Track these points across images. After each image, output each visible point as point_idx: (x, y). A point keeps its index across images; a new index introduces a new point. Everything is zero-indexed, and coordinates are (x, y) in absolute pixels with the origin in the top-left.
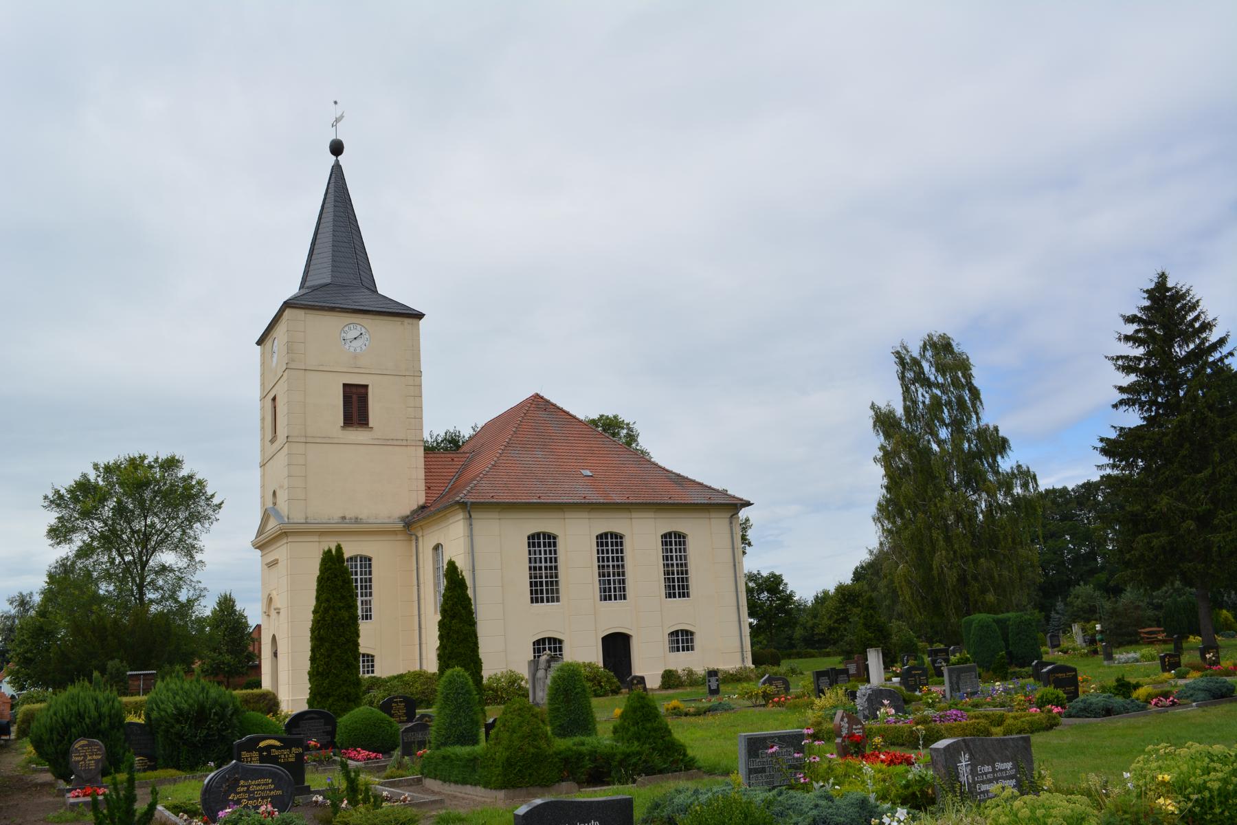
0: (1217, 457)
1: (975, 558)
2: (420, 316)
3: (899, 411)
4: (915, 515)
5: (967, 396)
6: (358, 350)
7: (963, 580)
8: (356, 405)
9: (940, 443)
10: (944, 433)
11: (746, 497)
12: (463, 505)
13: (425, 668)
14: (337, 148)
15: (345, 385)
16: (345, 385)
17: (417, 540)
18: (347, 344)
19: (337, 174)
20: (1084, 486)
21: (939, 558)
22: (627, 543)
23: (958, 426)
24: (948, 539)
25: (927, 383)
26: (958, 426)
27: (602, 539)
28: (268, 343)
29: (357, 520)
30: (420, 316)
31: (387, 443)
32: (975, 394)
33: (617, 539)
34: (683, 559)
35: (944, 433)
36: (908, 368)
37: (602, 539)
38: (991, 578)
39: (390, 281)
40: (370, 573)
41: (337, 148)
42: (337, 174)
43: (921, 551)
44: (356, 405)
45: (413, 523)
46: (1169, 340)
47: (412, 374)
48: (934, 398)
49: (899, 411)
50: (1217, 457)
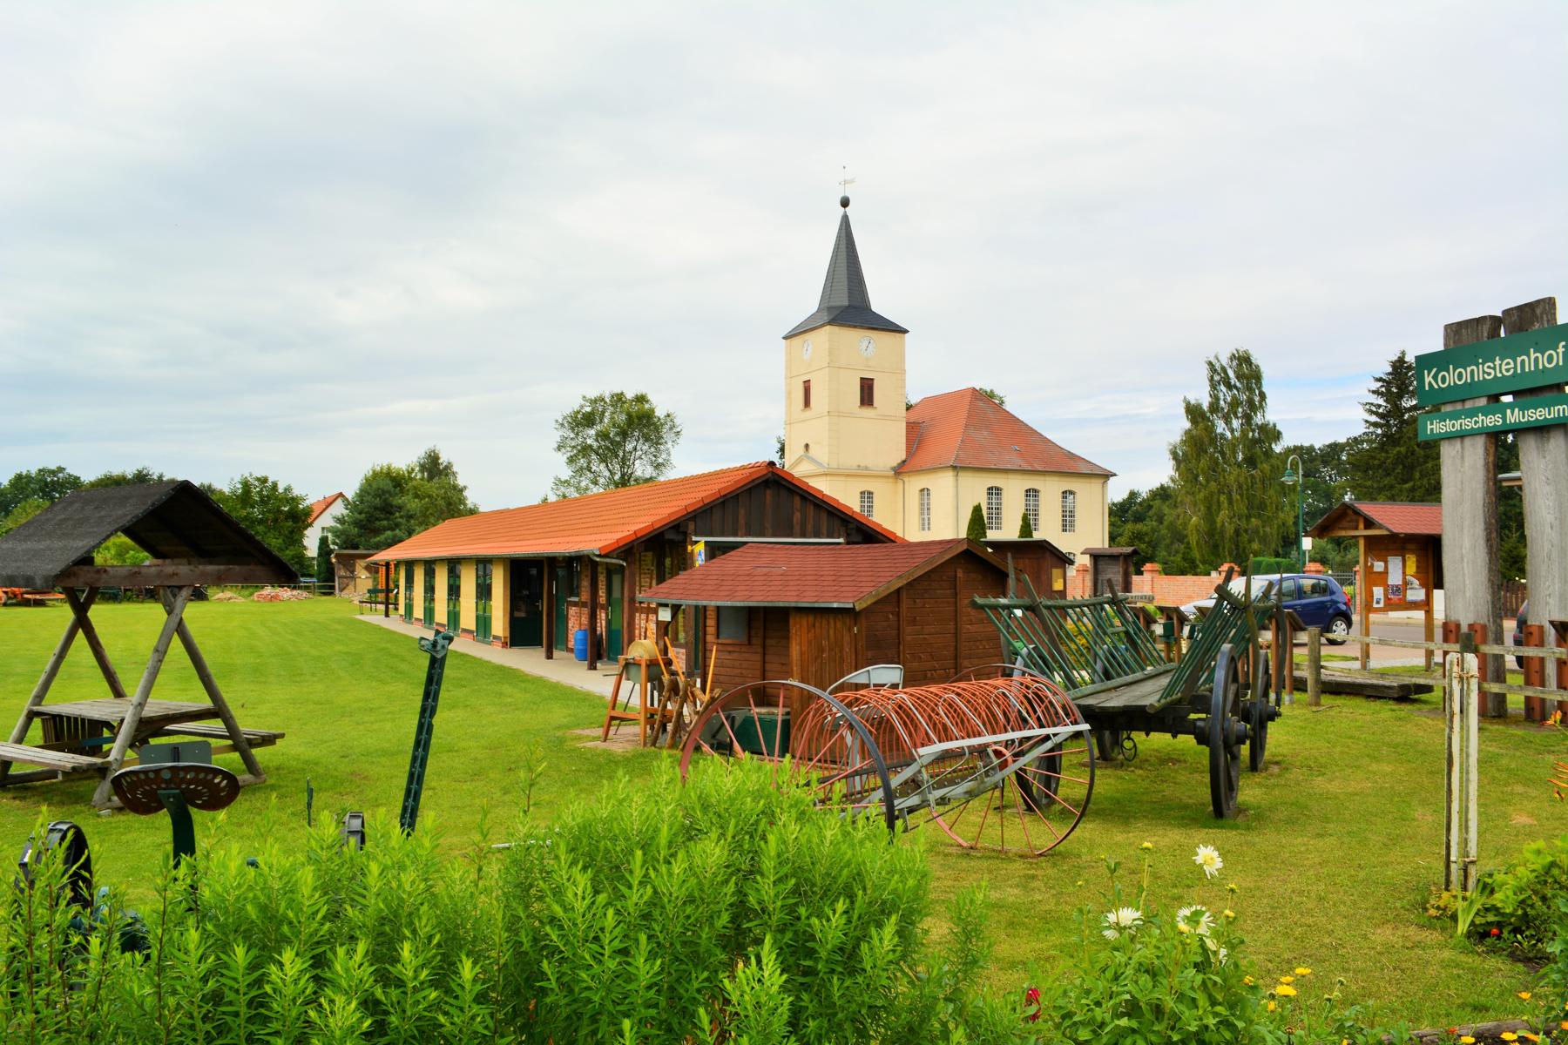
0: (1417, 475)
1: (1248, 518)
2: (905, 331)
3: (1205, 407)
4: (1208, 481)
5: (1257, 399)
7: (1237, 532)
8: (867, 392)
9: (1232, 431)
10: (1236, 423)
12: (954, 468)
14: (845, 203)
18: (859, 345)
20: (1330, 446)
21: (1223, 516)
22: (1004, 493)
23: (1248, 418)
24: (1230, 502)
25: (1229, 386)
26: (1248, 418)
28: (797, 341)
29: (866, 468)
30: (905, 331)
31: (884, 417)
32: (1263, 396)
35: (1236, 423)
36: (1217, 376)
38: (1257, 532)
39: (879, 303)
41: (845, 203)
43: (1209, 508)
44: (867, 392)
45: (900, 471)
46: (1400, 396)
48: (1234, 397)
49: (1205, 407)
50: (1417, 475)
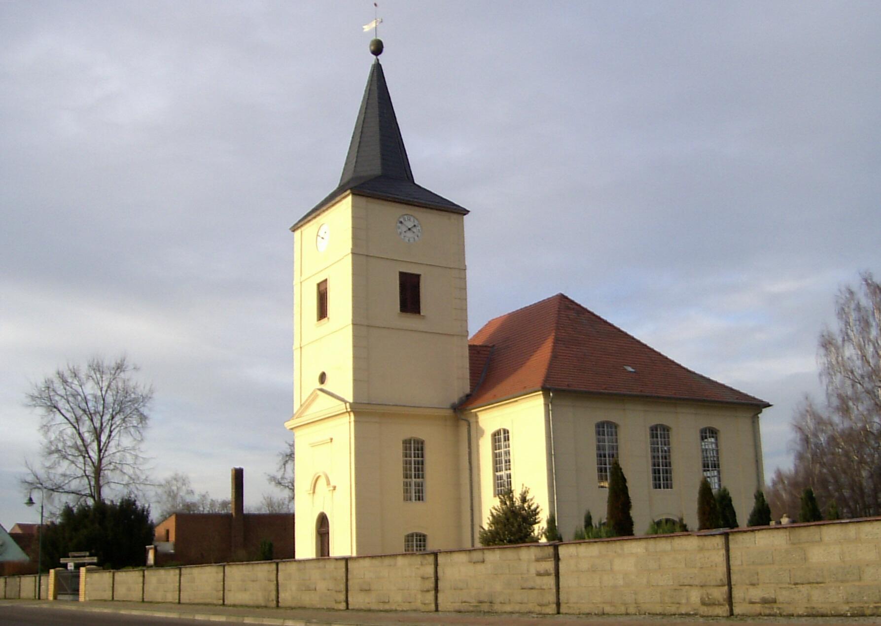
2: (465, 212)
6: (412, 240)
11: (766, 400)
13: (177, 571)
14: (378, 49)
15: (402, 275)
16: (402, 275)
17: (469, 425)
19: (378, 72)
27: (654, 429)
30: (465, 212)
33: (666, 429)
34: (667, 457)
37: (654, 429)
39: (423, 176)
40: (617, 442)
41: (378, 49)
42: (378, 72)
44: (410, 294)
47: (458, 270)
